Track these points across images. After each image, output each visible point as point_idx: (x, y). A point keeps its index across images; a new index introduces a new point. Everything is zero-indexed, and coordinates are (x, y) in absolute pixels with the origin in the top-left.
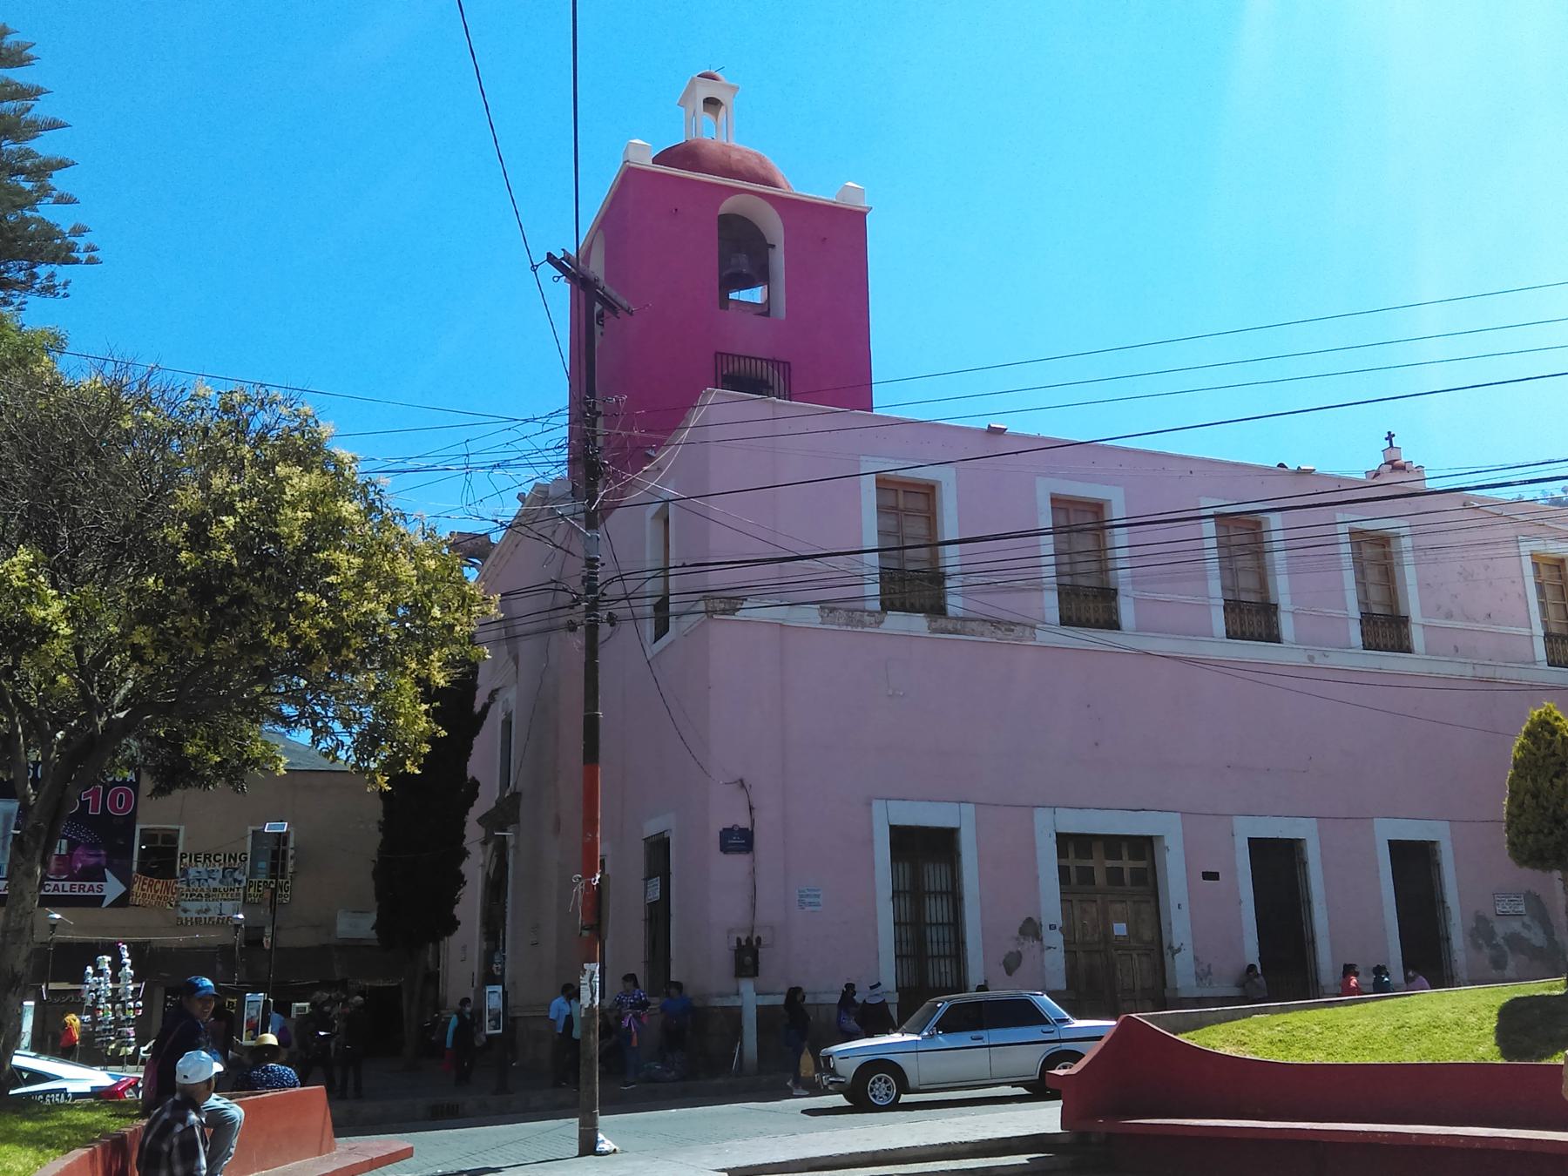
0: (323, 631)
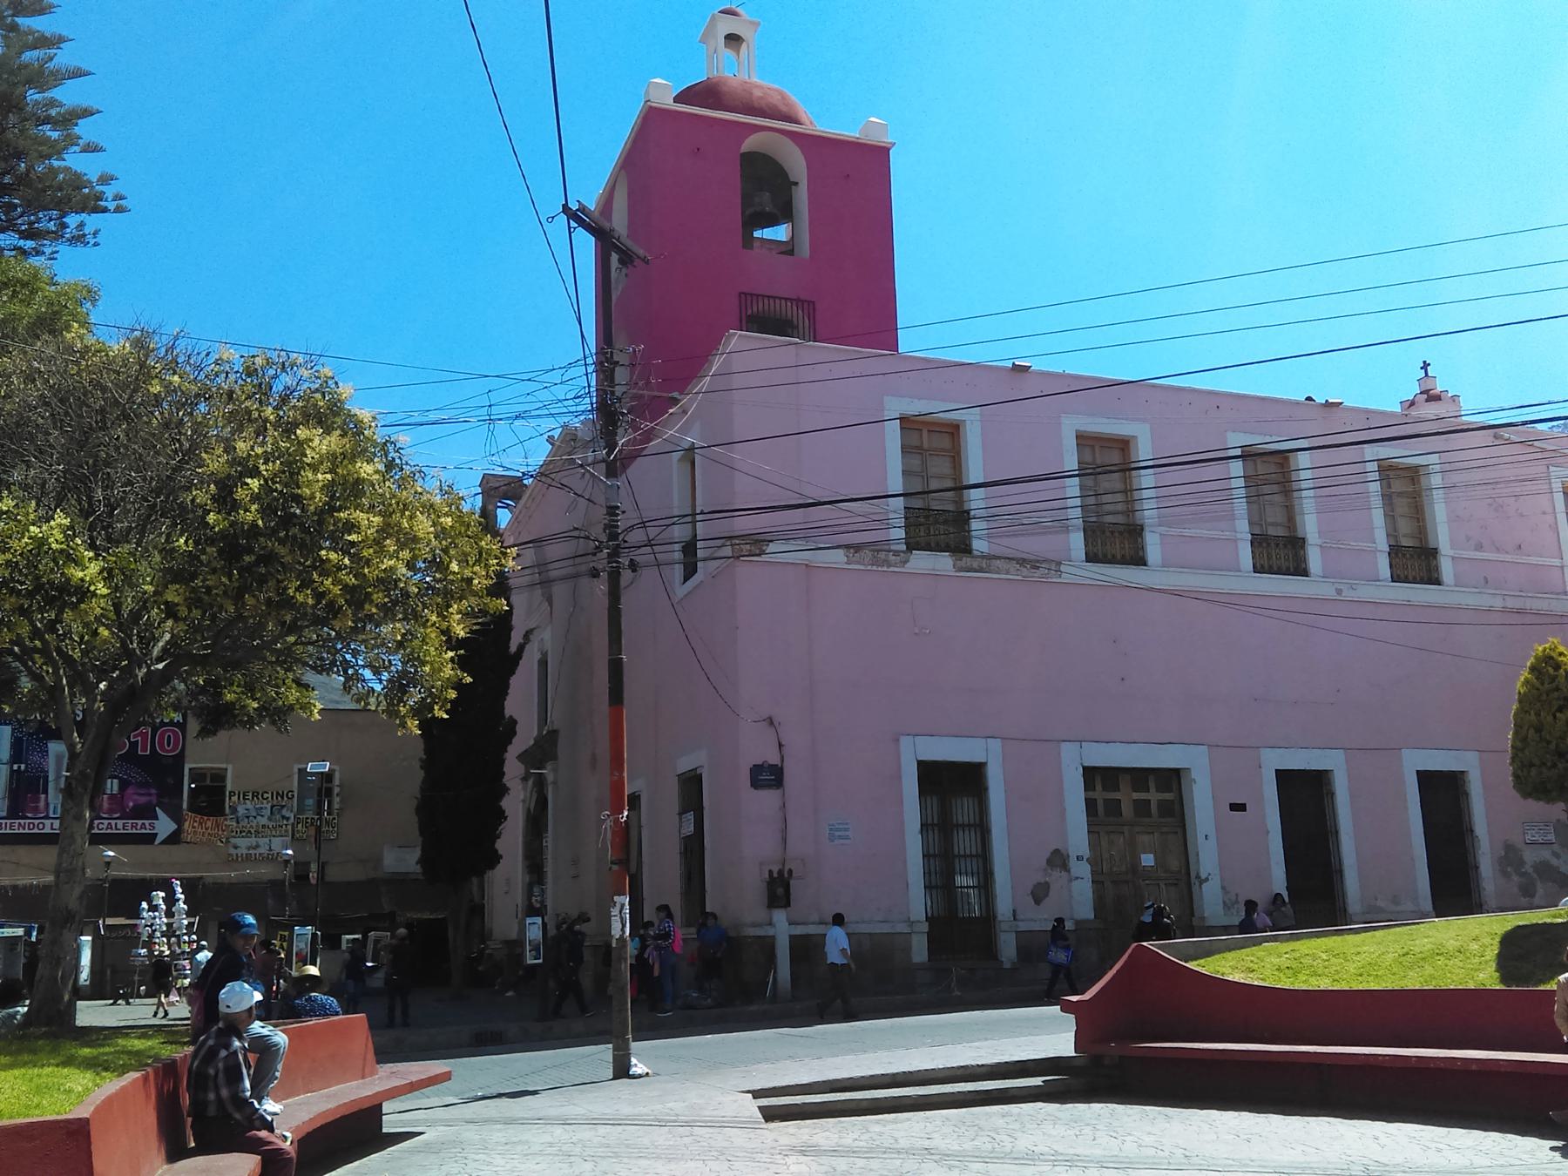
0: (345, 588)
